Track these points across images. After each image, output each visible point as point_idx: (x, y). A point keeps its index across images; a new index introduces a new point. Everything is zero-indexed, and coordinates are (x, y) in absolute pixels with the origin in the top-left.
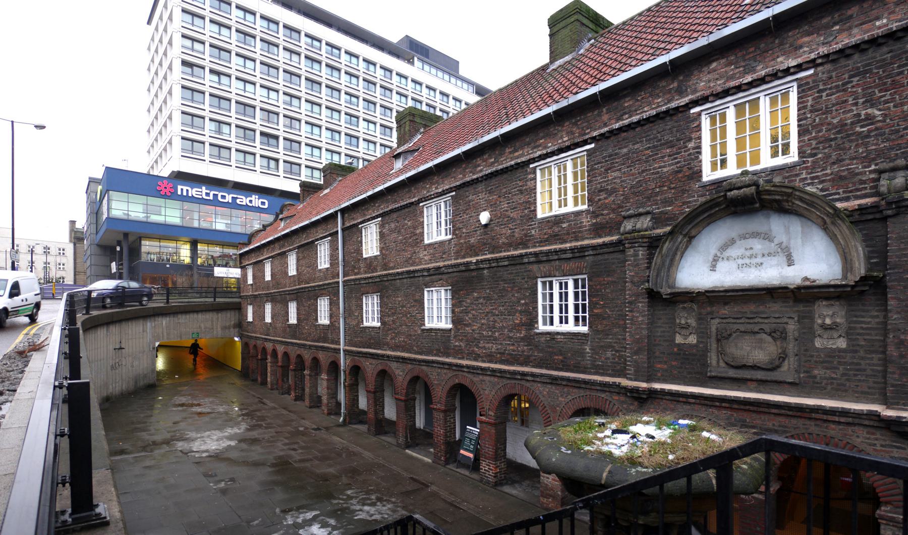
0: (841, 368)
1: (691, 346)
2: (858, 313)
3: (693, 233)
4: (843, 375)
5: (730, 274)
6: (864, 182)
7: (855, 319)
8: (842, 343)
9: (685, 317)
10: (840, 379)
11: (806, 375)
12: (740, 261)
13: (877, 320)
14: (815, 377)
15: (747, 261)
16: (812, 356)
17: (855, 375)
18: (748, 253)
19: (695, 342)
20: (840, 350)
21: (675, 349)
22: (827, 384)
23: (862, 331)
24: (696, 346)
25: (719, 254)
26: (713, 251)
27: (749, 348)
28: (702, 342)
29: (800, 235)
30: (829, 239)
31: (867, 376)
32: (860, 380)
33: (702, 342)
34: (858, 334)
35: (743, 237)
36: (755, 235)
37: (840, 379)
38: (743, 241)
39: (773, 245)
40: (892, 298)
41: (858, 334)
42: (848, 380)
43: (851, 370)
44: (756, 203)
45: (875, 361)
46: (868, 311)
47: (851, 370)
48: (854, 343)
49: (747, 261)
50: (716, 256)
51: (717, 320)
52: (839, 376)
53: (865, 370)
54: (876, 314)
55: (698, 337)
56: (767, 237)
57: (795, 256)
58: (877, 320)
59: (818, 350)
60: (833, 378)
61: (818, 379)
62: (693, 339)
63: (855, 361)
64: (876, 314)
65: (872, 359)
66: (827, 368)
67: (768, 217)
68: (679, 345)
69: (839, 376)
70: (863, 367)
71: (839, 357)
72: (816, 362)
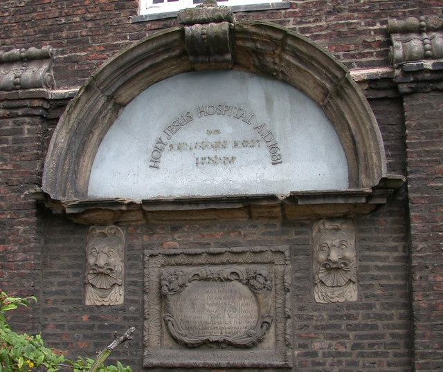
0: (352, 335)
1: (114, 310)
2: (371, 244)
3: (123, 96)
4: (355, 346)
6: (368, 45)
7: (367, 253)
8: (351, 294)
10: (350, 355)
11: (303, 351)
12: (201, 153)
13: (395, 254)
14: (315, 354)
15: (211, 153)
16: (310, 318)
17: (371, 345)
18: (212, 139)
19: (121, 301)
20: (350, 305)
22: (332, 365)
23: (376, 273)
24: (123, 309)
26: (155, 132)
27: (213, 309)
28: (133, 301)
31: (386, 346)
32: (376, 354)
33: (133, 301)
34: (373, 278)
36: (222, 109)
37: (350, 355)
38: (204, 118)
40: (415, 216)
41: (373, 278)
42: (362, 355)
44: (227, 52)
45: (395, 321)
46: (383, 240)
48: (368, 292)
50: (160, 141)
52: (349, 350)
53: (383, 336)
54: (394, 244)
55: (127, 292)
56: (242, 115)
57: (282, 151)
59: (317, 307)
60: (339, 354)
61: (320, 359)
63: (369, 322)
64: (394, 244)
65: (391, 317)
66: (332, 338)
68: (90, 309)
69: (349, 350)
70: (380, 331)
71: (349, 317)
72: (316, 328)
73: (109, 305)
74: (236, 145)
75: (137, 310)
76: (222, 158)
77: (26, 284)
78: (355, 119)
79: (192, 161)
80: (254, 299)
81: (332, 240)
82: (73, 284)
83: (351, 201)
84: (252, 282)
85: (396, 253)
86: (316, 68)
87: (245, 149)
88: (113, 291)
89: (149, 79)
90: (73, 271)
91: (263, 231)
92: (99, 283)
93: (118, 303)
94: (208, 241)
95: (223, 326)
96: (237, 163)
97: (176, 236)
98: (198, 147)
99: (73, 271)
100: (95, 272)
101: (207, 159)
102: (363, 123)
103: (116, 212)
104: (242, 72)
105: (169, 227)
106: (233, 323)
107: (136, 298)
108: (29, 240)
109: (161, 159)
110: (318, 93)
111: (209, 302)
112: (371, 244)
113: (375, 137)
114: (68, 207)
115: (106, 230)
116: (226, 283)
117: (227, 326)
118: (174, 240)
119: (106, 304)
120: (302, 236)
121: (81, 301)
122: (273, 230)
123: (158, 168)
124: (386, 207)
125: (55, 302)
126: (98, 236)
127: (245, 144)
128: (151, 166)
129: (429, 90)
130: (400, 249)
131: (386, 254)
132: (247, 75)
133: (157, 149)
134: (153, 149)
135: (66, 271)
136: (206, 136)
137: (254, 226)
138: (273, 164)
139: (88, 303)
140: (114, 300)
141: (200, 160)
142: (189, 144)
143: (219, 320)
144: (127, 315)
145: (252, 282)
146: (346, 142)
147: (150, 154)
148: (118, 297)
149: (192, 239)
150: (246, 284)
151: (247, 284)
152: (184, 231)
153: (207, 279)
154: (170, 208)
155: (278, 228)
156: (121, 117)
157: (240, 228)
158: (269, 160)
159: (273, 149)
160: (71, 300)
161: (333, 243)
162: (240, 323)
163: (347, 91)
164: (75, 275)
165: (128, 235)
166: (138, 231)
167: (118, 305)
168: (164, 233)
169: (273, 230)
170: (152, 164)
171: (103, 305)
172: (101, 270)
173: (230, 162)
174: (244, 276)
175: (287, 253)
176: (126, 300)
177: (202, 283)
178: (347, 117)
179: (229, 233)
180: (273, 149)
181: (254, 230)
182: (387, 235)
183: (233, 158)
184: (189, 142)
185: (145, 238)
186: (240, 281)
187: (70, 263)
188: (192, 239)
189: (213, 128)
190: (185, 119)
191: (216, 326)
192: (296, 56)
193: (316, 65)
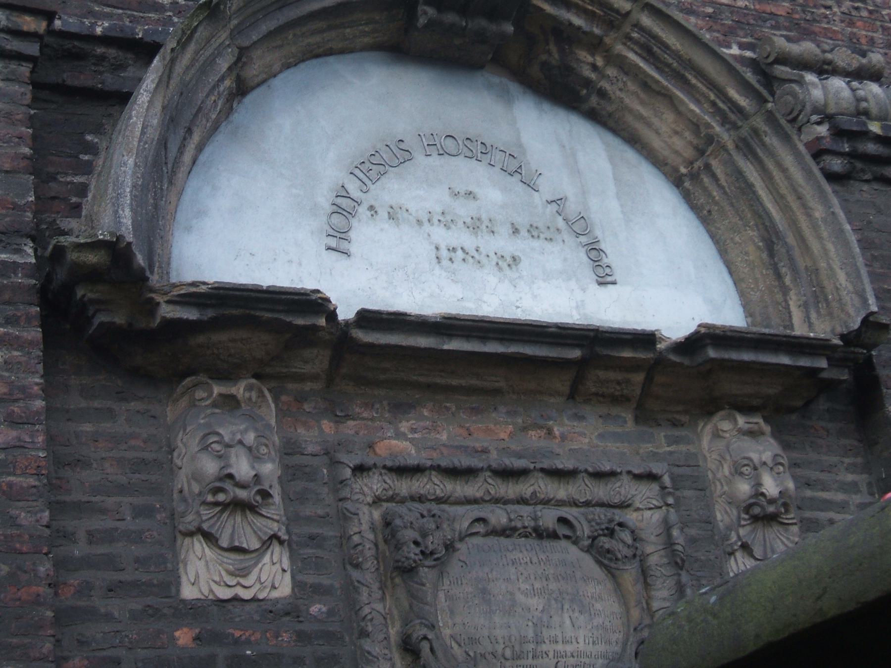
1: (270, 612)
5: (392, 269)
9: (228, 440)
12: (441, 235)
15: (467, 240)
18: (464, 210)
19: (285, 589)
21: (184, 637)
24: (289, 611)
25: (353, 188)
26: (331, 172)
27: (536, 603)
28: (319, 591)
29: (612, 189)
30: (663, 177)
33: (319, 591)
35: (443, 145)
36: (478, 150)
38: (435, 160)
39: (537, 199)
43: (794, 269)
46: (829, 469)
47: (794, 269)
49: (467, 240)
50: (343, 193)
51: (375, 484)
54: (850, 477)
55: (300, 565)
56: (516, 168)
57: (612, 257)
58: (97, 523)
62: (273, 577)
64: (850, 477)
67: (507, 99)
68: (195, 611)
73: (254, 599)
74: (516, 231)
75: (331, 613)
76: (492, 255)
77: (24, 518)
78: (779, 199)
79: (425, 251)
80: (609, 585)
81: (760, 453)
82: (136, 538)
83: (804, 362)
84: (606, 542)
85: (859, 496)
86: (693, 87)
87: (536, 244)
88: (267, 559)
89: (312, 40)
90: (135, 500)
91: (600, 431)
92: (228, 531)
93: (275, 594)
94: (485, 444)
95: (560, 647)
96: (524, 264)
97: (404, 426)
98: (435, 221)
99: (135, 500)
100: (221, 497)
101: (460, 253)
102: (804, 206)
103: (278, 335)
104: (505, 80)
105: (385, 403)
106: (581, 640)
107: (326, 581)
108: (23, 389)
109: (353, 235)
110: (678, 145)
111: (524, 586)
112: (814, 475)
113: (839, 233)
114: (169, 302)
115: (239, 389)
116: (547, 544)
117: (569, 648)
118: (399, 435)
119: (246, 595)
120: (683, 448)
121: (170, 584)
122: (619, 430)
123: (347, 254)
124: (481, 479)
125: (85, 589)
126: (214, 405)
127: (533, 231)
128: (329, 248)
129: (868, 176)
130: (864, 488)
131: (840, 497)
132: (514, 88)
133: (338, 210)
134: (329, 209)
135: (110, 501)
136: (447, 198)
137: (581, 418)
138: (601, 284)
139: (188, 592)
140: (268, 584)
141: (444, 253)
142: (412, 210)
143: (553, 633)
144: (306, 627)
145: (606, 542)
146: (747, 253)
147: (325, 219)
148: (279, 577)
149: (444, 437)
150: (588, 550)
151: (593, 548)
152: (422, 418)
153: (506, 532)
154: (423, 342)
155: (630, 426)
156: (236, 117)
157: (550, 419)
158: (588, 276)
159: (594, 251)
160: (135, 584)
161: (764, 459)
162: (594, 643)
163: (767, 140)
164: (145, 512)
165: (282, 413)
166: (307, 407)
167: (277, 600)
168: (373, 419)
169: (619, 430)
170: (333, 243)
171: (236, 599)
172: (242, 494)
173: (509, 265)
174: (585, 530)
175: (667, 480)
176: (297, 584)
177: (492, 541)
178: (762, 193)
179: (525, 429)
180: (594, 251)
181: (579, 426)
182: (834, 459)
183: (514, 258)
184: (412, 206)
185: (327, 426)
186: (575, 543)
187: (123, 480)
188: (444, 437)
189: (462, 188)
190: (382, 161)
191: (544, 647)
192: (648, 53)
193: (693, 81)
